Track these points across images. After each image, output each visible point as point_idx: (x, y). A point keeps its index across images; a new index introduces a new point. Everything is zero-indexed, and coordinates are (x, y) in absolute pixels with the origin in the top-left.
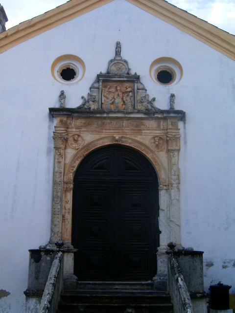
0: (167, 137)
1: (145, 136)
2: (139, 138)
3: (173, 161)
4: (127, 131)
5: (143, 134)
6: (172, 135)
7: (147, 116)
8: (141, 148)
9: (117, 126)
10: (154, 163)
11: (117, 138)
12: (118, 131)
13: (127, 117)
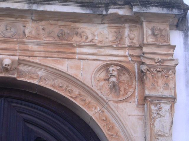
0: (143, 63)
1: (82, 63)
2: (65, 66)
3: (158, 126)
4: (35, 47)
5: (77, 56)
6: (154, 59)
7: (87, 11)
8: (71, 92)
9: (8, 34)
10: (105, 130)
11: (7, 61)
12: (12, 46)
13: (37, 11)
